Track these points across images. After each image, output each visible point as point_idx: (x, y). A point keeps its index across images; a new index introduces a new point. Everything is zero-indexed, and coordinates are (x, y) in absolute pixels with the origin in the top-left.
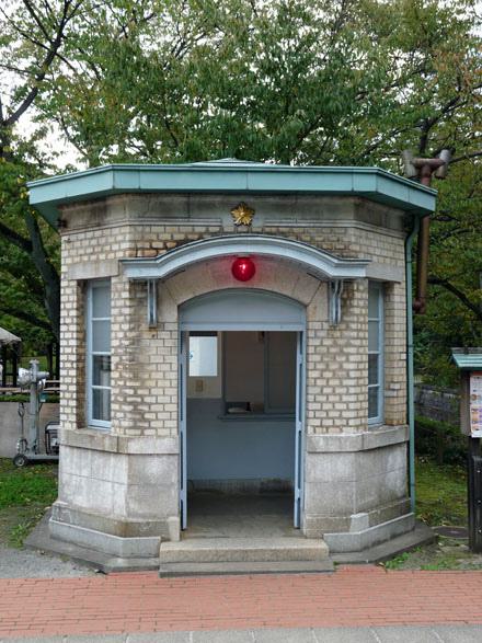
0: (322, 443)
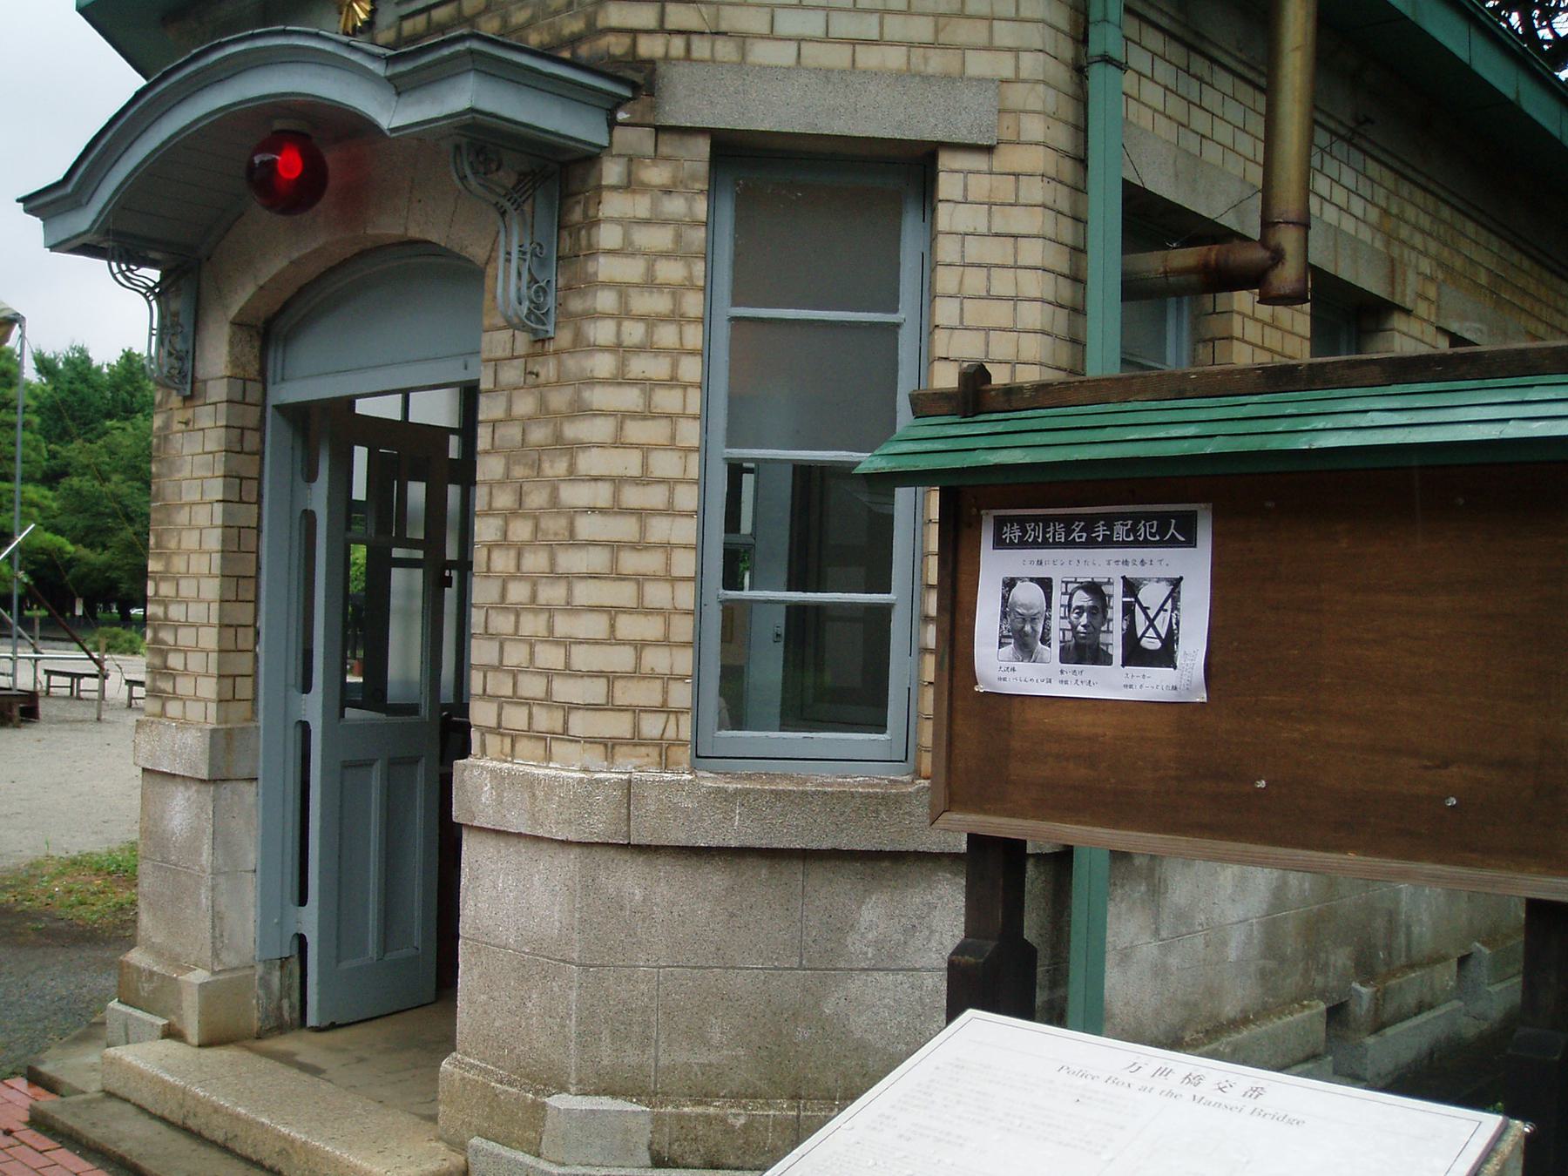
0: (487, 795)
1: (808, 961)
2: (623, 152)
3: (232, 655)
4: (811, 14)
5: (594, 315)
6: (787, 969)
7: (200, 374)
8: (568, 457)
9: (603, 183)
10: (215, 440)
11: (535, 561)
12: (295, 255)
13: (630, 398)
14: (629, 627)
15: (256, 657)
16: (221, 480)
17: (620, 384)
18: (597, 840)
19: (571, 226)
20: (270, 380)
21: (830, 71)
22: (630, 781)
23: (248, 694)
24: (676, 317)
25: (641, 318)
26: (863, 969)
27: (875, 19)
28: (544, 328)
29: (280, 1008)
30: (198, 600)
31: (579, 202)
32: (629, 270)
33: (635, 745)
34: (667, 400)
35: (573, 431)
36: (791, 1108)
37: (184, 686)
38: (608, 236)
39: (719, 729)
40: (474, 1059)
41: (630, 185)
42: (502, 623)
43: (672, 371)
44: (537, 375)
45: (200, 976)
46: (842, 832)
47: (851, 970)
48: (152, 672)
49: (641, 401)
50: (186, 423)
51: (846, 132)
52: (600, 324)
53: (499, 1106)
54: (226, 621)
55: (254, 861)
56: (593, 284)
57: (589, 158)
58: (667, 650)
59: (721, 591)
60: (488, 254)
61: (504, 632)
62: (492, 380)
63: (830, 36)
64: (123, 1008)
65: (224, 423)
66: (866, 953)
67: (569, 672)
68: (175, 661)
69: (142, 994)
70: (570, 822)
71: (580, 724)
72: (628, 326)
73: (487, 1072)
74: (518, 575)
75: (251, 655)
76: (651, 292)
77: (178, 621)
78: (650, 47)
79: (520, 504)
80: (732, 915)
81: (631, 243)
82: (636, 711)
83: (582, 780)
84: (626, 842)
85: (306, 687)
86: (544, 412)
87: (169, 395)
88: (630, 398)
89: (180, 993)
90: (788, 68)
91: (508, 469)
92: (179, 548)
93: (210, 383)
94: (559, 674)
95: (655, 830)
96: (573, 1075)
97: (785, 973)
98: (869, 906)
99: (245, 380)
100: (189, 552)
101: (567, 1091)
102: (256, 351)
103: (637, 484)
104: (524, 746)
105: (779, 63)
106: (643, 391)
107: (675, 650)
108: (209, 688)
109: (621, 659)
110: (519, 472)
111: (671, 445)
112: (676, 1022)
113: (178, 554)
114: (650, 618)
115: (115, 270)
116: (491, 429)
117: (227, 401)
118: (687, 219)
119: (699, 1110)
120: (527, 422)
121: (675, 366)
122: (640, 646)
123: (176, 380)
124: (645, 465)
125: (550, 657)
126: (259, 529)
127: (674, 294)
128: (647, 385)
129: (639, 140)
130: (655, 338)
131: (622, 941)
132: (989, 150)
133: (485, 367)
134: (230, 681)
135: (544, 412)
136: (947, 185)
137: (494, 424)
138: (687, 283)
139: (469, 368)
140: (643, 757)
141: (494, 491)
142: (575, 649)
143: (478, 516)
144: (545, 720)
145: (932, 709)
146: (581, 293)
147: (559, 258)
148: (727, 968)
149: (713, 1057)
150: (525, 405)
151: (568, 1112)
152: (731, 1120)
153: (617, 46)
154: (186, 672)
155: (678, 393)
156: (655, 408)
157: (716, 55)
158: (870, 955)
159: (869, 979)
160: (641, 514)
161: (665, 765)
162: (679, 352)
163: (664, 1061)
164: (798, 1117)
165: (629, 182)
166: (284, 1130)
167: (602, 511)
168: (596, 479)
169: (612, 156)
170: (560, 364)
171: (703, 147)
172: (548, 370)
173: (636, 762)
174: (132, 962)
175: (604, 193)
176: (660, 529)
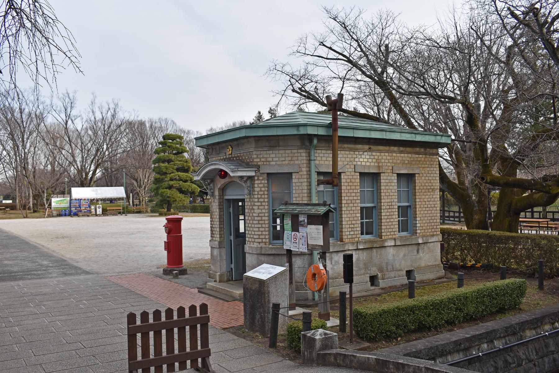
10: (217, 204)
11: (251, 222)
13: (259, 204)
14: (261, 229)
24: (264, 194)
34: (263, 204)
37: (215, 236)
41: (258, 179)
45: (219, 273)
67: (255, 235)
71: (256, 240)
78: (259, 163)
88: (259, 204)
104: (251, 243)
109: (260, 233)
111: (264, 209)
122: (262, 231)
128: (261, 202)
132: (298, 172)
136: (294, 177)
145: (539, 208)
161: (265, 245)
162: (264, 198)
171: (266, 175)
176: (264, 218)
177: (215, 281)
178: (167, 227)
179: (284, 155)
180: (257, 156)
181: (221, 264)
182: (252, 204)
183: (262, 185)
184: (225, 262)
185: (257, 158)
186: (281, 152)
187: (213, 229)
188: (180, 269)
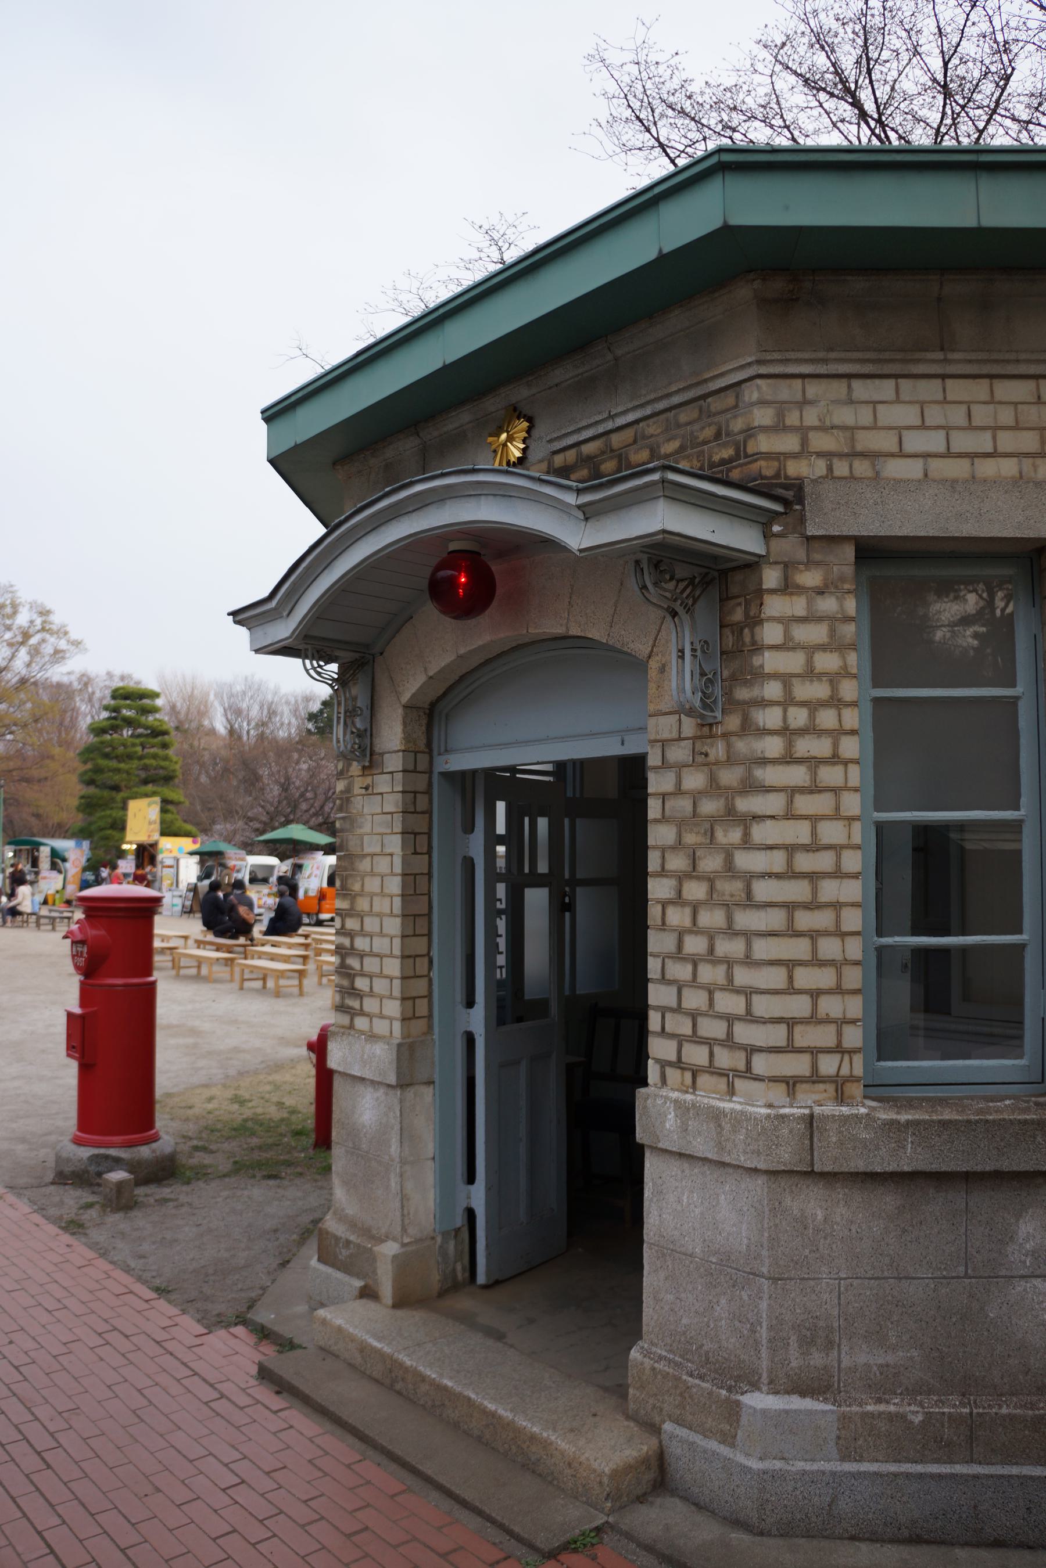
0: (671, 1121)
1: (973, 1270)
2: (780, 560)
3: (413, 981)
4: (933, 433)
5: (763, 703)
6: (953, 1278)
7: (377, 749)
8: (742, 827)
9: (764, 587)
10: (393, 803)
12: (462, 651)
13: (798, 775)
14: (805, 978)
15: (430, 981)
16: (399, 837)
17: (788, 763)
18: (783, 1168)
19: (732, 625)
20: (435, 753)
21: (955, 481)
22: (812, 1116)
23: (425, 1013)
24: (835, 702)
25: (803, 704)
26: (1023, 1277)
27: (988, 435)
28: (713, 714)
29: (454, 1270)
30: (381, 934)
31: (740, 604)
32: (792, 662)
33: (814, 1082)
34: (831, 775)
35: (744, 805)
36: (963, 1405)
37: (370, 1005)
38: (771, 633)
39: (879, 1060)
40: (661, 1349)
41: (787, 588)
42: (681, 971)
43: (834, 751)
44: (706, 755)
45: (390, 1249)
46: (1003, 1155)
47: (1012, 1277)
48: (340, 991)
49: (808, 778)
50: (367, 788)
51: (974, 533)
52: (768, 710)
53: (691, 1397)
54: (407, 953)
55: (433, 1151)
56: (760, 676)
57: (751, 565)
58: (839, 997)
59: (876, 938)
60: (650, 649)
61: (682, 979)
62: (660, 758)
63: (951, 451)
64: (322, 1267)
65: (400, 789)
66: (1025, 1262)
67: (750, 1017)
68: (361, 983)
69: (340, 1257)
70: (759, 1153)
71: (761, 1064)
72: (792, 711)
73: (678, 1365)
74: (695, 929)
75: (426, 980)
76: (812, 681)
77: (363, 951)
78: (794, 469)
79: (694, 867)
80: (904, 1231)
81: (792, 639)
82: (814, 1052)
83: (768, 1116)
84: (809, 1170)
85: (470, 1003)
86: (714, 787)
87: (350, 765)
88: (798, 775)
89: (374, 1260)
90: (919, 481)
91: (679, 835)
92: (363, 891)
93: (386, 756)
94: (739, 1018)
95: (836, 1158)
96: (765, 1375)
97: (952, 1281)
98: (1027, 1220)
99: (416, 753)
100: (372, 896)
101: (759, 1389)
102: (424, 728)
103: (808, 851)
105: (909, 476)
106: (809, 768)
107: (846, 997)
108: (393, 1008)
110: (690, 839)
111: (836, 815)
112: (855, 1328)
113: (361, 895)
114: (823, 969)
115: (309, 666)
116: (661, 800)
117: (403, 771)
118: (840, 616)
119: (882, 1407)
120: (696, 797)
121: (836, 745)
122: (815, 994)
123: (357, 753)
124: (814, 833)
125: (730, 1003)
126: (430, 874)
127: (831, 681)
128: (813, 763)
129: (789, 547)
130: (817, 721)
131: (806, 1257)
133: (652, 747)
134: (410, 1002)
135: (714, 787)
137: (664, 796)
138: (842, 672)
139: (626, 743)
140: (821, 1092)
141: (666, 855)
142: (756, 999)
143: (651, 876)
144: (724, 1059)
146: (747, 683)
147: (722, 653)
148: (901, 1278)
149: (891, 1359)
150: (694, 780)
151: (764, 1412)
152: (910, 1417)
153: (767, 468)
154: (371, 993)
155: (839, 769)
156: (820, 782)
157: (854, 472)
158: (1028, 1264)
159: (1028, 1285)
160: (813, 877)
161: (841, 1098)
162: (837, 734)
163: (846, 1362)
164: (971, 1413)
165: (787, 586)
166: (491, 1406)
167: (778, 876)
168: (771, 848)
169: (771, 564)
170: (729, 746)
171: (849, 552)
172: (718, 750)
173: (816, 1097)
174: (330, 1230)
175: (765, 596)
176: (829, 890)
177: (368, 1293)
178: (82, 942)
179: (982, 415)
180: (781, 415)
181: (409, 1185)
182: (729, 777)
183: (817, 633)
184: (429, 1174)
185: (779, 427)
186: (957, 389)
187: (353, 962)
188: (145, 1152)
